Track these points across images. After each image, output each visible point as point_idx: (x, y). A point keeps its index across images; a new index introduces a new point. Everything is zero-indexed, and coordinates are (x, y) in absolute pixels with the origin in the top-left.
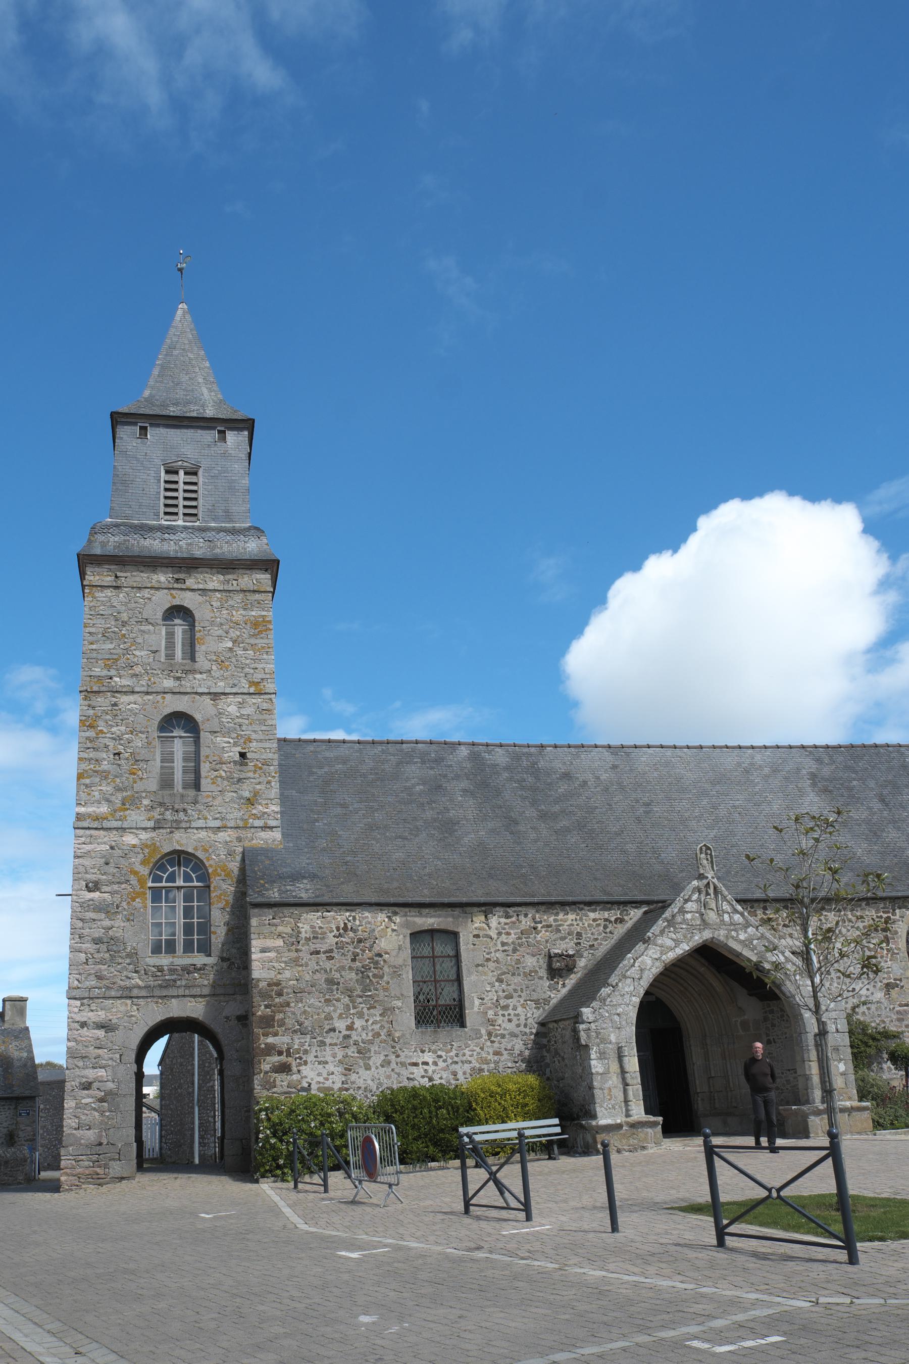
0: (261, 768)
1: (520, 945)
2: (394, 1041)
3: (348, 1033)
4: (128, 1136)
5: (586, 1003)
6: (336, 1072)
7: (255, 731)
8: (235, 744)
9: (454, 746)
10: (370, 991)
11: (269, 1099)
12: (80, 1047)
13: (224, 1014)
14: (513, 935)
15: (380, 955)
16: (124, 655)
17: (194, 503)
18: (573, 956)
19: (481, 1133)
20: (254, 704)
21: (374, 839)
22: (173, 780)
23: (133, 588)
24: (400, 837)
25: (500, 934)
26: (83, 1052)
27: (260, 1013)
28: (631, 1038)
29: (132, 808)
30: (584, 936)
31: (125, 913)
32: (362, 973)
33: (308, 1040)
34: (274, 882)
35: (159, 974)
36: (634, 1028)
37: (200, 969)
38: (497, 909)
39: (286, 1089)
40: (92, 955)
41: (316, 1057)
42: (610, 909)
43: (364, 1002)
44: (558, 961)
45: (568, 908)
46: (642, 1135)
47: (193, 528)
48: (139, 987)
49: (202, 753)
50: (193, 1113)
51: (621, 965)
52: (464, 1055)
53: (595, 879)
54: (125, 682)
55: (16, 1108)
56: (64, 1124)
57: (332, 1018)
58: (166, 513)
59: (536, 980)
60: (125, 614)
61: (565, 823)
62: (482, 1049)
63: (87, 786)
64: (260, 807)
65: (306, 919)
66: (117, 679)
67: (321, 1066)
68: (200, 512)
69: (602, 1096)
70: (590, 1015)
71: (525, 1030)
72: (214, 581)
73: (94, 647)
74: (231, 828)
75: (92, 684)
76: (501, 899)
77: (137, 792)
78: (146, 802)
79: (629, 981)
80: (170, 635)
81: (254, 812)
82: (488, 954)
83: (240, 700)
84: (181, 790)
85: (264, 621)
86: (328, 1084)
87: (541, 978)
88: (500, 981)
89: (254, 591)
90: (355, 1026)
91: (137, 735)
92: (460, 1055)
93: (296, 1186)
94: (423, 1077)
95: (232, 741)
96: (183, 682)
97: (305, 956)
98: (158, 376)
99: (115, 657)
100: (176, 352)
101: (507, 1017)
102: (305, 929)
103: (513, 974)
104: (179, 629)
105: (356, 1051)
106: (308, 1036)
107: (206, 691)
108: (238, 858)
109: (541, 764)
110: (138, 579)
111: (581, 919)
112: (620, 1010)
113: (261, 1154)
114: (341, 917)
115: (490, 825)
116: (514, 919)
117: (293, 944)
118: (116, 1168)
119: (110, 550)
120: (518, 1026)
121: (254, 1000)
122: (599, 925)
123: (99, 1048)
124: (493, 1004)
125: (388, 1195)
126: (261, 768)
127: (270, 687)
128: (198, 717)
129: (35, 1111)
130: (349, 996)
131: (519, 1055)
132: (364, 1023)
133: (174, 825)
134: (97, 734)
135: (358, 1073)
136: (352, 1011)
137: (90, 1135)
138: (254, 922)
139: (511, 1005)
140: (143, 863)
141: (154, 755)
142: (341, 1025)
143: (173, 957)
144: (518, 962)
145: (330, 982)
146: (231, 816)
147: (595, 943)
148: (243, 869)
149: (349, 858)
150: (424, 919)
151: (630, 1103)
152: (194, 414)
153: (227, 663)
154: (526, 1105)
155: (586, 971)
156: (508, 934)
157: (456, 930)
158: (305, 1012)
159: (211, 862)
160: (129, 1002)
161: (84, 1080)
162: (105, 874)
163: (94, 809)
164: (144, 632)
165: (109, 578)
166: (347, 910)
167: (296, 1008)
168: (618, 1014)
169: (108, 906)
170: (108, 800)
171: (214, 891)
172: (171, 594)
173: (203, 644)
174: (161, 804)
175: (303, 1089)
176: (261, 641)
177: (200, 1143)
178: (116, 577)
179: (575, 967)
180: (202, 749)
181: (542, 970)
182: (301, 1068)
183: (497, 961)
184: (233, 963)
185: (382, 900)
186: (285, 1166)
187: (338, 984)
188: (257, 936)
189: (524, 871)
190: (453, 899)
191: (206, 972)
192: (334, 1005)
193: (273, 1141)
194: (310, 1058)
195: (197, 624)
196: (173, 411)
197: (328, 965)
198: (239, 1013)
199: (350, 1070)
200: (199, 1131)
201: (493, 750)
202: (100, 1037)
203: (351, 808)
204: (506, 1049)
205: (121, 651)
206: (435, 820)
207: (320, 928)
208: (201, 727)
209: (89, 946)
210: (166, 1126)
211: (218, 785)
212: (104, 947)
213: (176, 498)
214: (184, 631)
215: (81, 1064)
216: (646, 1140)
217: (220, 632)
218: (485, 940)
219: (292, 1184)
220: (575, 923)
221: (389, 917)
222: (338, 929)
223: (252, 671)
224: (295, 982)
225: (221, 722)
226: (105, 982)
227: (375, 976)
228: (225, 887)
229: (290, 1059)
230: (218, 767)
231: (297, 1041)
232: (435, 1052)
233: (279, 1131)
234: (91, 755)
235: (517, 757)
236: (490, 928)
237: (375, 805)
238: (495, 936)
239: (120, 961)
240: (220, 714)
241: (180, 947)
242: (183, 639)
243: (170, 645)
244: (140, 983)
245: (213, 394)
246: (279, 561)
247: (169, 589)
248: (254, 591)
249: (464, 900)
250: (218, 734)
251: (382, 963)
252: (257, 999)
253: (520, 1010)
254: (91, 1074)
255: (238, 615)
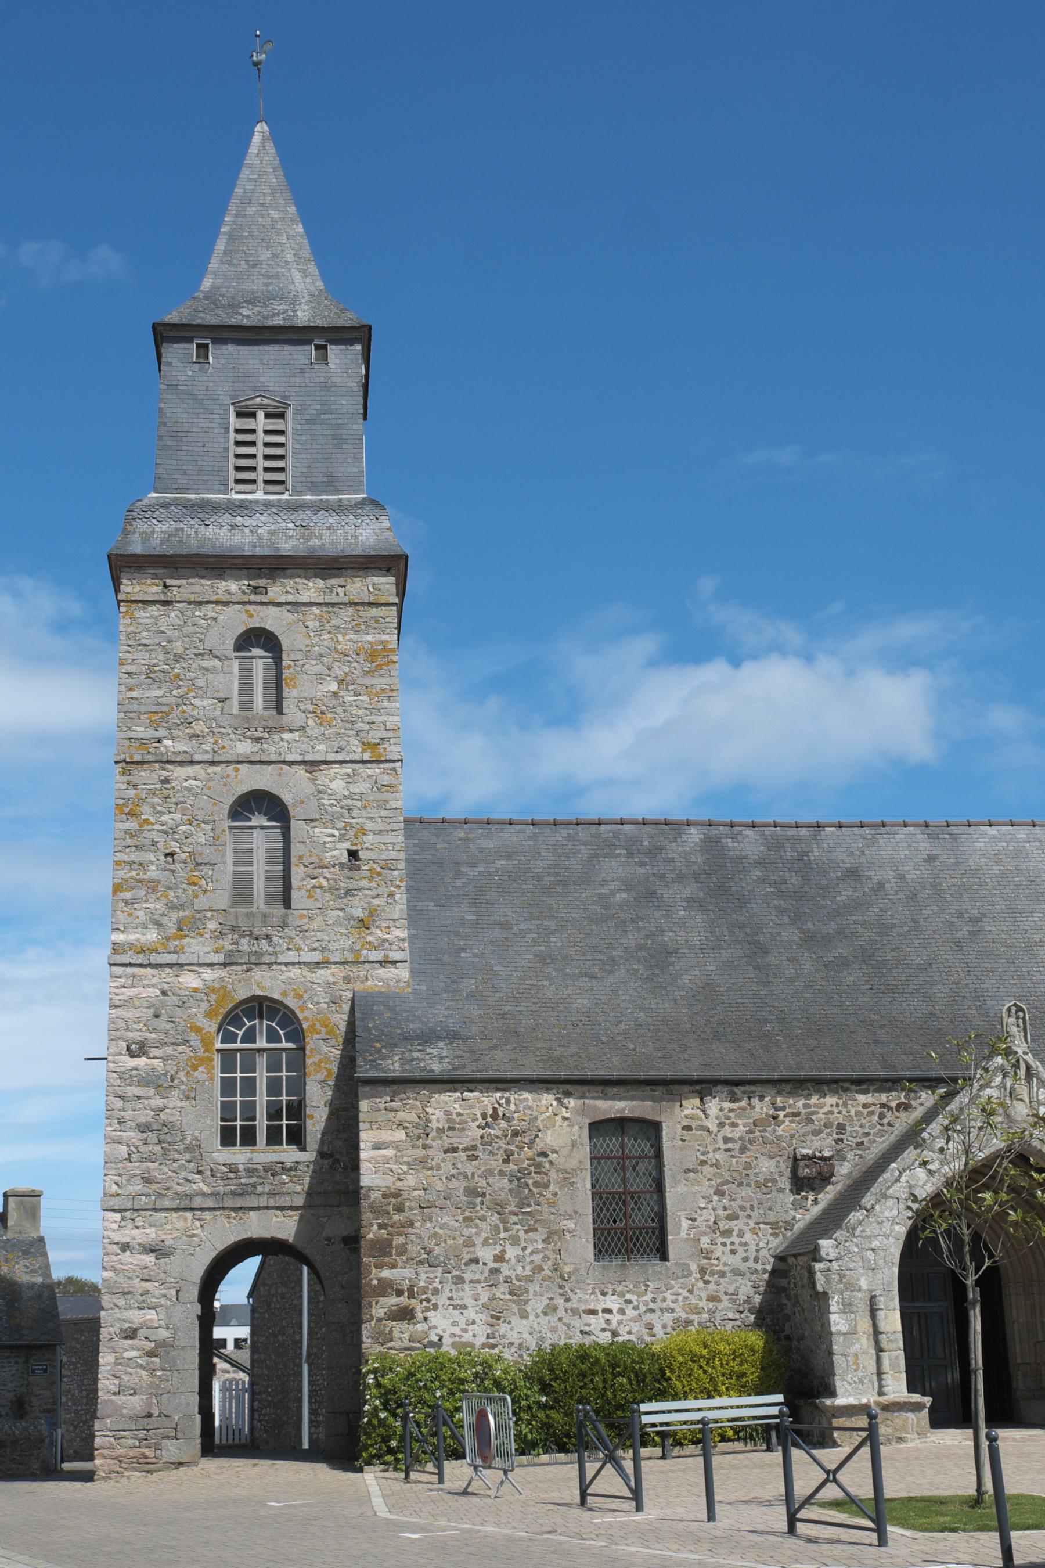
0: (379, 874)
1: (752, 1142)
2: (564, 1279)
3: (496, 1265)
4: (188, 1404)
5: (826, 1234)
6: (478, 1321)
7: (371, 818)
8: (342, 838)
9: (675, 827)
10: (529, 1205)
11: (382, 1357)
12: (120, 1279)
13: (324, 1234)
14: (741, 1127)
15: (544, 1155)
16: (178, 705)
17: (279, 464)
18: (829, 1159)
19: (654, 1413)
20: (370, 776)
21: (547, 978)
22: (251, 891)
23: (190, 603)
24: (586, 975)
25: (721, 1125)
26: (125, 1286)
27: (371, 1236)
28: (890, 1283)
29: (192, 934)
30: (848, 1129)
31: (183, 1087)
32: (519, 1179)
33: (439, 1274)
34: (395, 1045)
35: (232, 1175)
36: (896, 1270)
37: (290, 1169)
38: (719, 1088)
39: (407, 1344)
40: (136, 1148)
41: (451, 1299)
42: (889, 1090)
43: (520, 1222)
44: (807, 1166)
45: (825, 1088)
46: (898, 1422)
47: (278, 504)
48: (204, 1195)
49: (293, 853)
50: (300, 1374)
51: (881, 1179)
52: (664, 1300)
53: (876, 1042)
54: (180, 747)
55: (26, 1362)
56: (100, 1386)
57: (474, 1245)
58: (238, 481)
59: (774, 1193)
60: (179, 644)
61: (841, 950)
62: (691, 1292)
63: (127, 902)
64: (378, 932)
65: (438, 1102)
66: (168, 743)
67: (457, 1312)
68: (289, 477)
69: (844, 1365)
70: (831, 1250)
71: (755, 1266)
72: (311, 589)
73: (134, 694)
74: (336, 963)
75: (133, 750)
76: (723, 1074)
77: (199, 912)
78: (212, 925)
79: (890, 1202)
80: (246, 673)
81: (369, 938)
82: (703, 1154)
83: (349, 771)
84: (262, 906)
85: (384, 649)
86: (467, 1337)
87: (781, 1190)
88: (720, 1193)
89: (370, 604)
90: (507, 1257)
91: (198, 825)
92: (658, 1300)
93: (407, 1476)
94: (603, 1330)
95: (337, 833)
96: (265, 746)
97: (437, 1155)
98: (225, 253)
99: (165, 709)
100: (251, 210)
101: (729, 1247)
102: (437, 1117)
103: (740, 1184)
104: (260, 662)
105: (507, 1291)
106: (440, 1269)
107: (299, 758)
108: (346, 1007)
109: (815, 854)
110: (197, 589)
111: (845, 1105)
112: (875, 1244)
113: (366, 1434)
114: (487, 1100)
115: (725, 954)
116: (743, 1103)
117: (419, 1138)
118: (172, 1450)
119: (156, 545)
120: (746, 1259)
121: (363, 1217)
122: (872, 1113)
123: (147, 1280)
124: (709, 1227)
125: (502, 1483)
126: (379, 874)
127: (393, 750)
128: (287, 798)
129: (55, 1367)
130: (499, 1213)
131: (745, 1302)
132: (520, 1253)
133: (253, 959)
134: (141, 825)
135: (509, 1323)
136: (502, 1235)
137: (135, 1403)
138: (364, 1105)
139: (736, 1229)
140: (208, 1015)
141: (224, 856)
142: (486, 1254)
143: (252, 1152)
144: (748, 1166)
145: (472, 1192)
146: (336, 945)
147: (866, 1140)
148: (351, 1024)
149: (507, 1008)
150: (610, 1102)
151: (884, 1376)
152: (278, 321)
153: (330, 716)
154: (743, 1375)
155: (849, 1182)
156: (734, 1125)
157: (657, 1119)
158: (435, 1235)
159: (307, 1014)
160: (189, 1215)
161: (127, 1325)
162: (154, 1031)
163: (138, 936)
164: (207, 670)
165: (155, 589)
166: (498, 1090)
167: (422, 1229)
168: (873, 1250)
169: (159, 1077)
170: (158, 924)
171: (312, 1055)
172: (247, 611)
173: (294, 687)
174: (234, 929)
175: (431, 1344)
176: (381, 680)
177: (311, 1422)
178: (165, 586)
179: (832, 1175)
180: (292, 846)
181: (784, 1179)
182: (428, 1314)
183: (717, 1165)
184: (338, 1160)
185: (549, 1074)
186: (398, 1450)
187: (483, 1195)
188: (368, 1126)
189: (769, 1027)
190: (653, 1074)
191: (299, 1173)
192: (477, 1226)
193: (382, 1415)
194: (442, 1300)
195: (284, 657)
196: (248, 316)
197: (469, 1168)
198: (345, 1233)
199: (498, 1318)
200: (310, 1402)
201: (740, 833)
202: (149, 1264)
203: (515, 930)
204: (726, 1293)
205: (173, 700)
206: (640, 947)
207: (459, 1114)
208: (292, 814)
209: (132, 1135)
210: (259, 1393)
211: (317, 900)
212: (153, 1137)
213: (253, 456)
214: (266, 668)
215: (121, 1302)
216: (904, 1428)
217: (319, 668)
218: (698, 1135)
219: (402, 1475)
220: (836, 1110)
221: (558, 1100)
222: (484, 1116)
223: (367, 727)
224: (422, 1193)
225: (321, 806)
226: (155, 1187)
227: (536, 1184)
228: (325, 1049)
229: (413, 1301)
230: (316, 872)
231: (423, 1276)
232: (621, 1295)
233: (390, 1399)
234: (133, 857)
235: (776, 845)
236: (707, 1116)
237: (552, 924)
238: (714, 1128)
239: (176, 1156)
240: (320, 792)
241: (262, 1135)
242: (265, 678)
243: (246, 688)
244: (205, 1189)
245: (308, 280)
246: (407, 557)
247: (243, 603)
248: (370, 604)
249: (669, 1074)
250: (317, 823)
251: (547, 1165)
252: (366, 1215)
253: (748, 1237)
254: (136, 1317)
255: (346, 641)
